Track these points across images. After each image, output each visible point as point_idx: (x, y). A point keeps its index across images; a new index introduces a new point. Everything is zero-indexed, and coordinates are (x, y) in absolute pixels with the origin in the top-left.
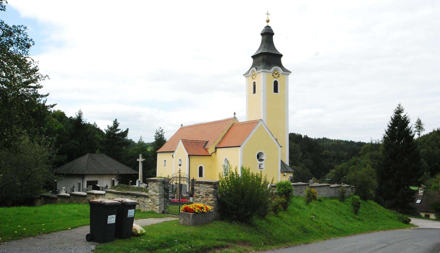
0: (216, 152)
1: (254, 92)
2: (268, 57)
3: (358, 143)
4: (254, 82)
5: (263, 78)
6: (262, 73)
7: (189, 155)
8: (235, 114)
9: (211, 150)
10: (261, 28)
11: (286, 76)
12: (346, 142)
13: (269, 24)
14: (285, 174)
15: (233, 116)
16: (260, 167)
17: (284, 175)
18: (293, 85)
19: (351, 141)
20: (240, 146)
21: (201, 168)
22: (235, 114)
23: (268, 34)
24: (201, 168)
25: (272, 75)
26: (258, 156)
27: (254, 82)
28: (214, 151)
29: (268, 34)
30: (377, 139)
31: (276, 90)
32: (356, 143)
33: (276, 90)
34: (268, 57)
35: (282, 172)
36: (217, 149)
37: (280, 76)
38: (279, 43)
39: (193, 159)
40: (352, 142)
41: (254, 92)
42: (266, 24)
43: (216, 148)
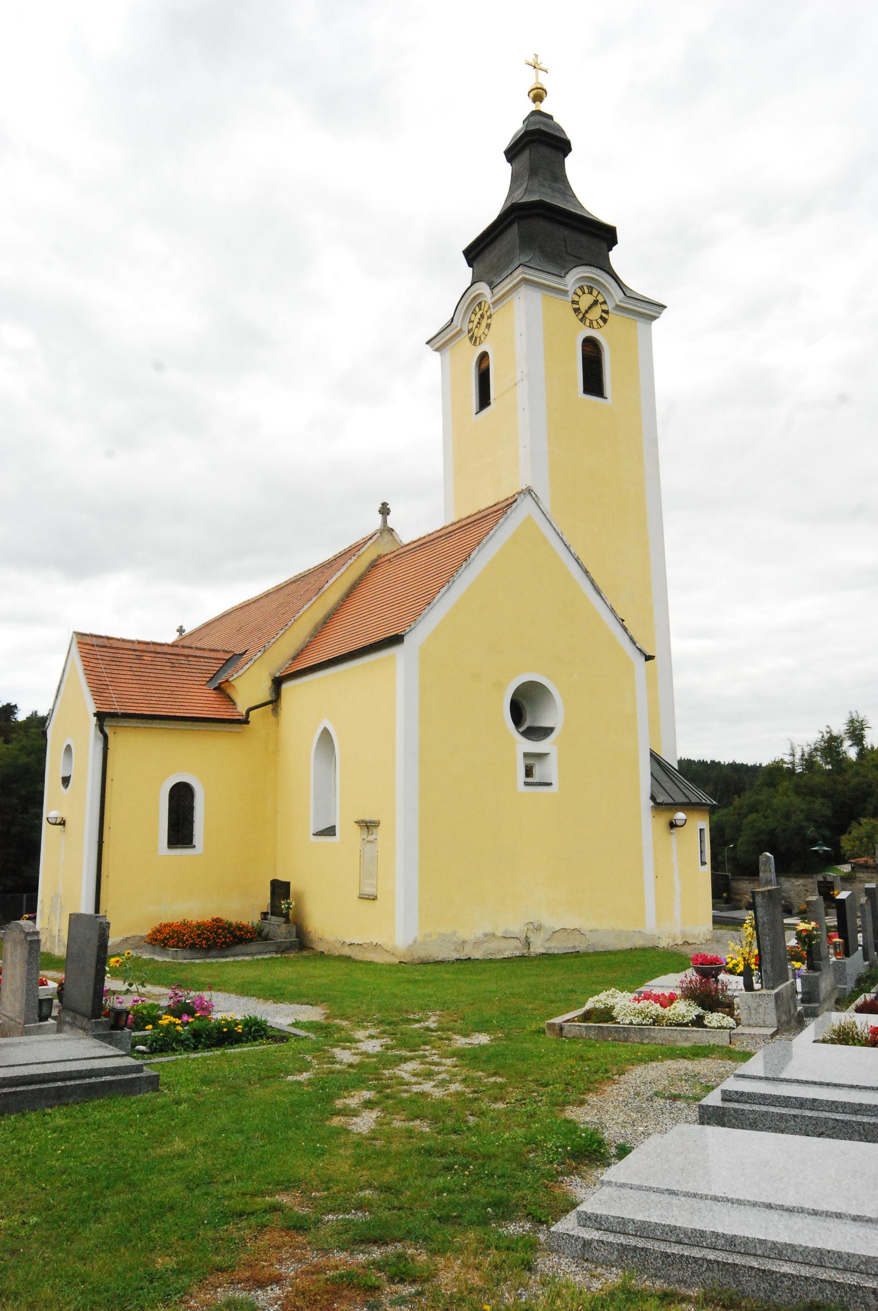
0: (275, 700)
1: (484, 400)
2: (543, 228)
3: (729, 765)
4: (484, 356)
5: (532, 321)
6: (523, 290)
7: (101, 717)
8: (385, 510)
9: (250, 687)
10: (512, 127)
11: (640, 324)
12: (702, 763)
13: (544, 107)
14: (680, 816)
15: (376, 521)
16: (529, 772)
17: (673, 825)
18: (675, 362)
19: (713, 762)
20: (396, 640)
21: (181, 799)
22: (385, 510)
23: (540, 146)
24: (181, 799)
25: (569, 308)
26: (517, 712)
27: (484, 356)
28: (264, 693)
29: (540, 146)
30: (804, 744)
31: (593, 383)
32: (724, 765)
33: (593, 383)
34: (543, 228)
35: (658, 806)
36: (286, 687)
37: (611, 318)
38: (592, 185)
39: (128, 743)
40: (715, 765)
41: (484, 400)
42: (533, 107)
43: (278, 683)
